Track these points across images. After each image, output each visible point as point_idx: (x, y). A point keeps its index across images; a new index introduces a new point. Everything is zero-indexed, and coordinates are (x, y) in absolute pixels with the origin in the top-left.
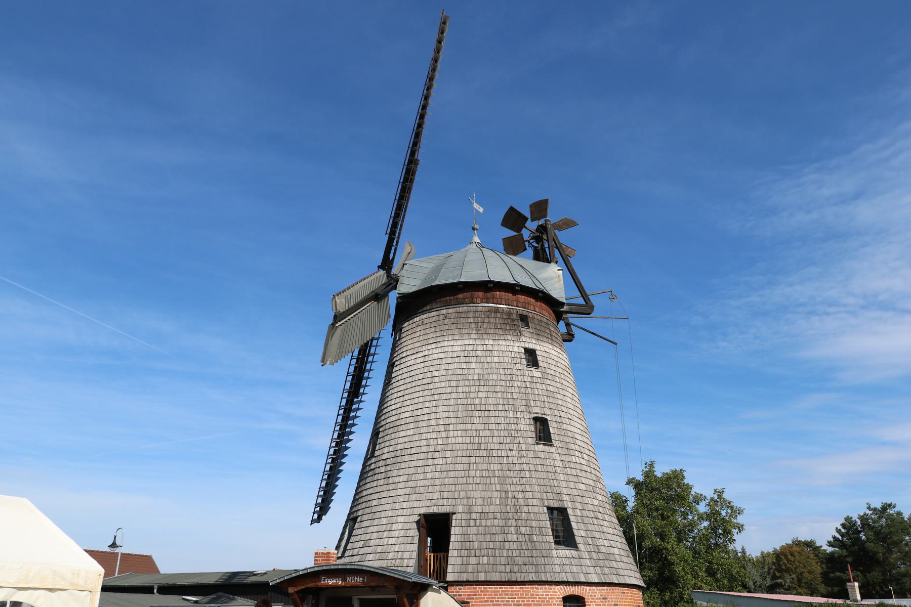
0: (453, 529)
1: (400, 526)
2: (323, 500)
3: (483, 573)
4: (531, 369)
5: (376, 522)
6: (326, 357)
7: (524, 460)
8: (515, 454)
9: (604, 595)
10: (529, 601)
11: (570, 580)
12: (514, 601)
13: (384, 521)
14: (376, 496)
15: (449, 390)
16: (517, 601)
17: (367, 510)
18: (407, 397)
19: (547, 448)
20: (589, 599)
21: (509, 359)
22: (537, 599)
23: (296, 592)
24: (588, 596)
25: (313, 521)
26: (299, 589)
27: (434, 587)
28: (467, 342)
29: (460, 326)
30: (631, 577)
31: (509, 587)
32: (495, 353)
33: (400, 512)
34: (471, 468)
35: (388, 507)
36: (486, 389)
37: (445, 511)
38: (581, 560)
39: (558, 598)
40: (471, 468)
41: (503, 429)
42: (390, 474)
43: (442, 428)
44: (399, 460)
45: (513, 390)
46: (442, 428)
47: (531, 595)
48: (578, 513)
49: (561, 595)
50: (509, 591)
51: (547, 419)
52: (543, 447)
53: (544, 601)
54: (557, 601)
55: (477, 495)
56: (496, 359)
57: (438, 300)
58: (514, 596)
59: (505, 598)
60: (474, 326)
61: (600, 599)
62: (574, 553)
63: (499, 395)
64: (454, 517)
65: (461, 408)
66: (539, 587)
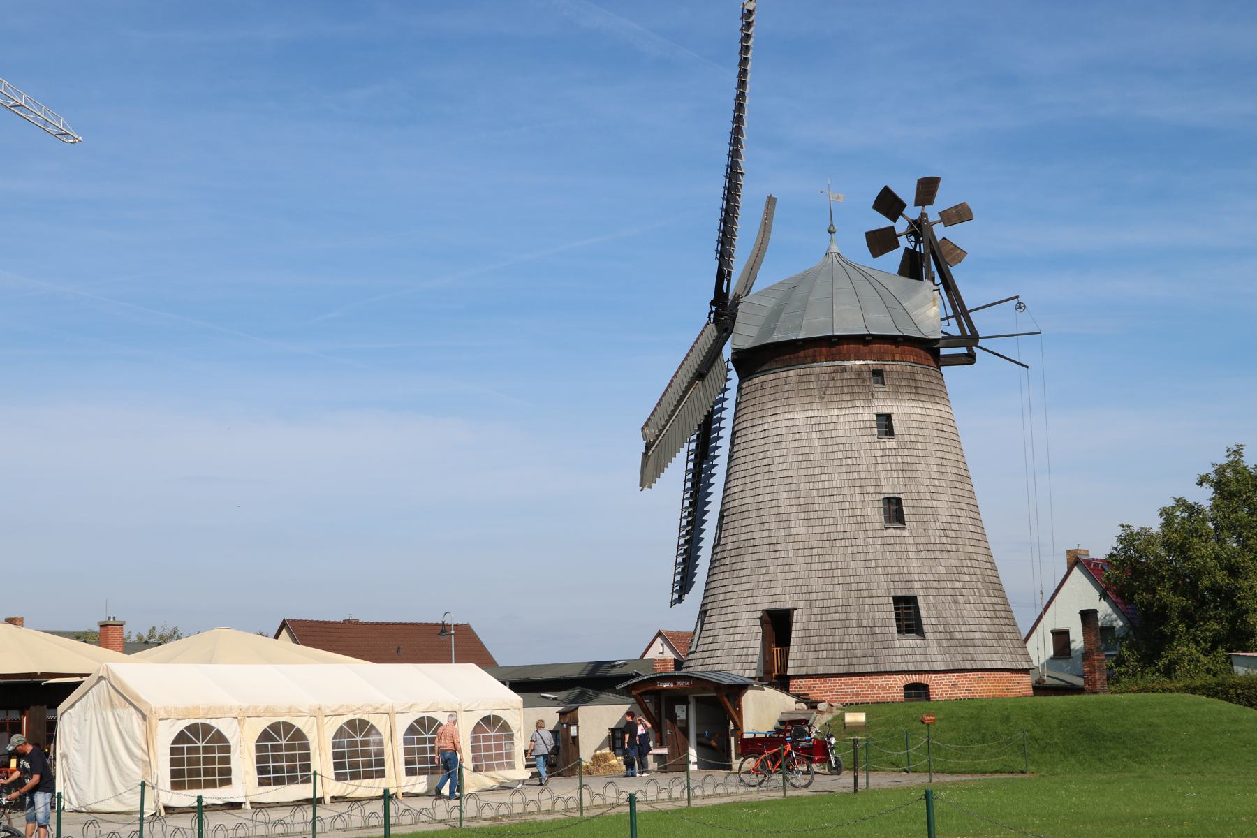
0: (794, 625)
1: (744, 623)
2: (682, 578)
4: (883, 440)
5: (722, 618)
6: (644, 481)
7: (871, 549)
8: (861, 542)
10: (868, 691)
13: (730, 617)
14: (723, 589)
15: (790, 473)
16: (856, 691)
17: (715, 605)
18: (748, 479)
21: (858, 430)
23: (639, 694)
25: (673, 602)
26: (641, 691)
27: (754, 685)
28: (809, 414)
31: (848, 678)
32: (840, 426)
33: (744, 608)
35: (732, 602)
36: (830, 470)
39: (898, 687)
42: (734, 567)
43: (784, 518)
44: (743, 551)
48: (931, 599)
50: (848, 683)
52: (894, 531)
55: (819, 589)
56: (841, 433)
57: (777, 359)
60: (816, 392)
62: (919, 642)
63: (844, 477)
64: (795, 612)
65: (803, 494)
66: (879, 677)
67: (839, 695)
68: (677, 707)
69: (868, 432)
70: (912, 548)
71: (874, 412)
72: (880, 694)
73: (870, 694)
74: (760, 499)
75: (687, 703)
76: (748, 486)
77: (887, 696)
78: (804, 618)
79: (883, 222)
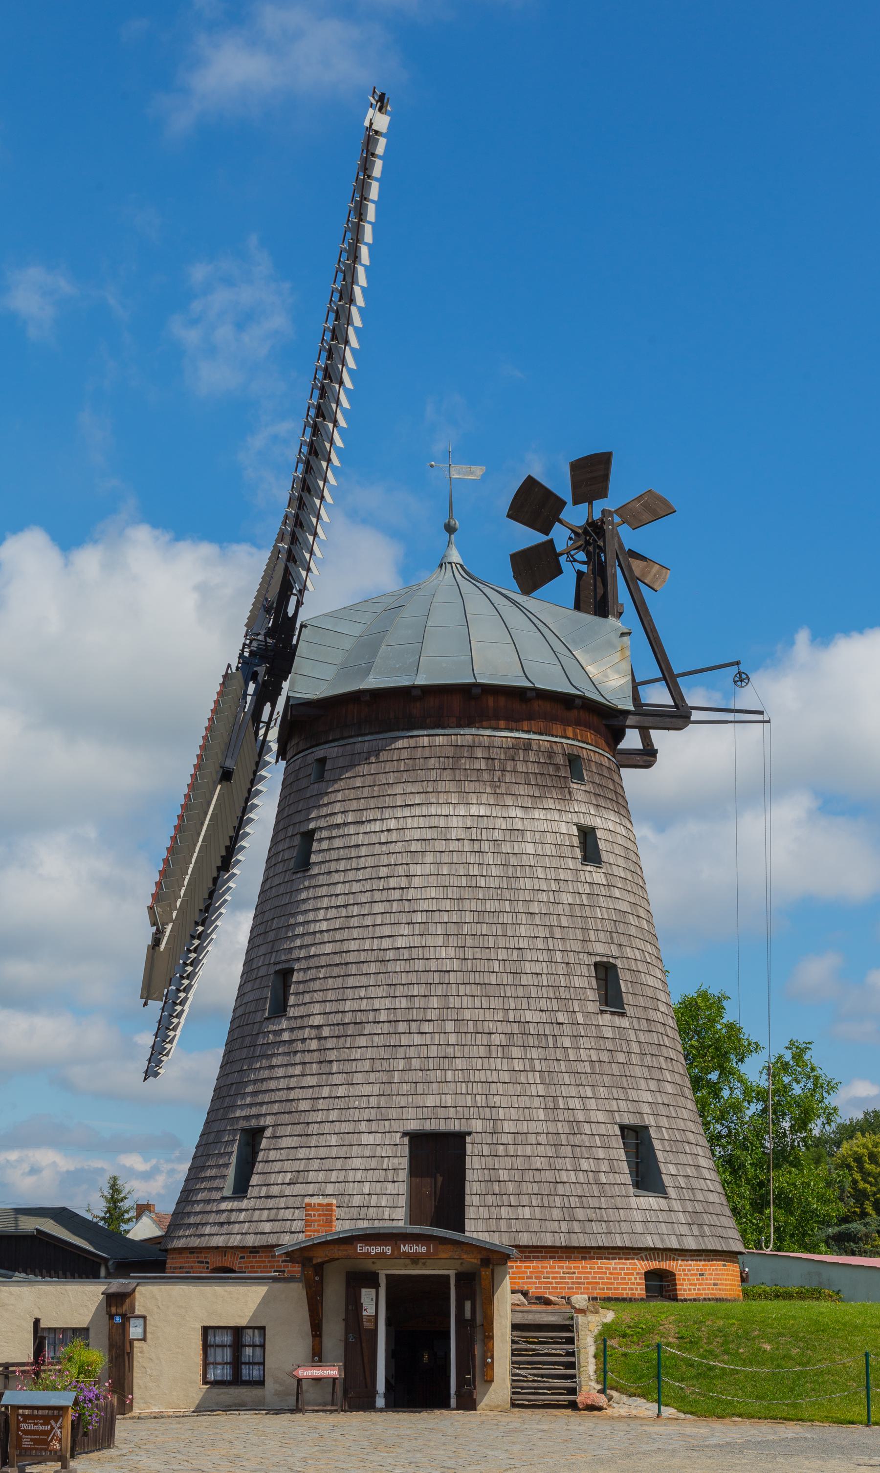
3: (525, 1233)
4: (589, 868)
9: (702, 1270)
10: (595, 1278)
11: (658, 1247)
12: (572, 1278)
16: (578, 1278)
19: (618, 1021)
20: (681, 1275)
22: (608, 1275)
24: (679, 1270)
28: (474, 810)
29: (460, 775)
30: (730, 1240)
34: (494, 1055)
37: (453, 1128)
38: (672, 1213)
39: (638, 1274)
40: (494, 1055)
41: (545, 984)
45: (559, 909)
46: (436, 978)
47: (598, 1268)
49: (643, 1269)
51: (615, 966)
53: (618, 1279)
54: (636, 1279)
58: (573, 1270)
59: (558, 1273)
61: (696, 1275)
62: (663, 1203)
64: (468, 1139)
67: (551, 1283)
68: (364, 1291)
69: (567, 852)
70: (635, 1048)
71: (576, 821)
72: (612, 1284)
73: (598, 1283)
74: (386, 943)
75: (376, 1286)
76: (354, 922)
77: (623, 1289)
78: (486, 1150)
79: (562, 488)
